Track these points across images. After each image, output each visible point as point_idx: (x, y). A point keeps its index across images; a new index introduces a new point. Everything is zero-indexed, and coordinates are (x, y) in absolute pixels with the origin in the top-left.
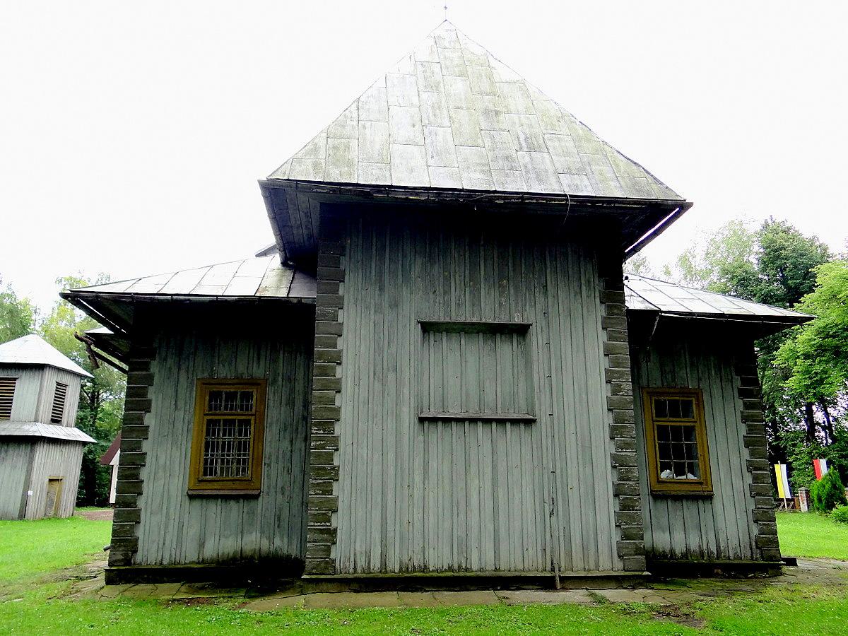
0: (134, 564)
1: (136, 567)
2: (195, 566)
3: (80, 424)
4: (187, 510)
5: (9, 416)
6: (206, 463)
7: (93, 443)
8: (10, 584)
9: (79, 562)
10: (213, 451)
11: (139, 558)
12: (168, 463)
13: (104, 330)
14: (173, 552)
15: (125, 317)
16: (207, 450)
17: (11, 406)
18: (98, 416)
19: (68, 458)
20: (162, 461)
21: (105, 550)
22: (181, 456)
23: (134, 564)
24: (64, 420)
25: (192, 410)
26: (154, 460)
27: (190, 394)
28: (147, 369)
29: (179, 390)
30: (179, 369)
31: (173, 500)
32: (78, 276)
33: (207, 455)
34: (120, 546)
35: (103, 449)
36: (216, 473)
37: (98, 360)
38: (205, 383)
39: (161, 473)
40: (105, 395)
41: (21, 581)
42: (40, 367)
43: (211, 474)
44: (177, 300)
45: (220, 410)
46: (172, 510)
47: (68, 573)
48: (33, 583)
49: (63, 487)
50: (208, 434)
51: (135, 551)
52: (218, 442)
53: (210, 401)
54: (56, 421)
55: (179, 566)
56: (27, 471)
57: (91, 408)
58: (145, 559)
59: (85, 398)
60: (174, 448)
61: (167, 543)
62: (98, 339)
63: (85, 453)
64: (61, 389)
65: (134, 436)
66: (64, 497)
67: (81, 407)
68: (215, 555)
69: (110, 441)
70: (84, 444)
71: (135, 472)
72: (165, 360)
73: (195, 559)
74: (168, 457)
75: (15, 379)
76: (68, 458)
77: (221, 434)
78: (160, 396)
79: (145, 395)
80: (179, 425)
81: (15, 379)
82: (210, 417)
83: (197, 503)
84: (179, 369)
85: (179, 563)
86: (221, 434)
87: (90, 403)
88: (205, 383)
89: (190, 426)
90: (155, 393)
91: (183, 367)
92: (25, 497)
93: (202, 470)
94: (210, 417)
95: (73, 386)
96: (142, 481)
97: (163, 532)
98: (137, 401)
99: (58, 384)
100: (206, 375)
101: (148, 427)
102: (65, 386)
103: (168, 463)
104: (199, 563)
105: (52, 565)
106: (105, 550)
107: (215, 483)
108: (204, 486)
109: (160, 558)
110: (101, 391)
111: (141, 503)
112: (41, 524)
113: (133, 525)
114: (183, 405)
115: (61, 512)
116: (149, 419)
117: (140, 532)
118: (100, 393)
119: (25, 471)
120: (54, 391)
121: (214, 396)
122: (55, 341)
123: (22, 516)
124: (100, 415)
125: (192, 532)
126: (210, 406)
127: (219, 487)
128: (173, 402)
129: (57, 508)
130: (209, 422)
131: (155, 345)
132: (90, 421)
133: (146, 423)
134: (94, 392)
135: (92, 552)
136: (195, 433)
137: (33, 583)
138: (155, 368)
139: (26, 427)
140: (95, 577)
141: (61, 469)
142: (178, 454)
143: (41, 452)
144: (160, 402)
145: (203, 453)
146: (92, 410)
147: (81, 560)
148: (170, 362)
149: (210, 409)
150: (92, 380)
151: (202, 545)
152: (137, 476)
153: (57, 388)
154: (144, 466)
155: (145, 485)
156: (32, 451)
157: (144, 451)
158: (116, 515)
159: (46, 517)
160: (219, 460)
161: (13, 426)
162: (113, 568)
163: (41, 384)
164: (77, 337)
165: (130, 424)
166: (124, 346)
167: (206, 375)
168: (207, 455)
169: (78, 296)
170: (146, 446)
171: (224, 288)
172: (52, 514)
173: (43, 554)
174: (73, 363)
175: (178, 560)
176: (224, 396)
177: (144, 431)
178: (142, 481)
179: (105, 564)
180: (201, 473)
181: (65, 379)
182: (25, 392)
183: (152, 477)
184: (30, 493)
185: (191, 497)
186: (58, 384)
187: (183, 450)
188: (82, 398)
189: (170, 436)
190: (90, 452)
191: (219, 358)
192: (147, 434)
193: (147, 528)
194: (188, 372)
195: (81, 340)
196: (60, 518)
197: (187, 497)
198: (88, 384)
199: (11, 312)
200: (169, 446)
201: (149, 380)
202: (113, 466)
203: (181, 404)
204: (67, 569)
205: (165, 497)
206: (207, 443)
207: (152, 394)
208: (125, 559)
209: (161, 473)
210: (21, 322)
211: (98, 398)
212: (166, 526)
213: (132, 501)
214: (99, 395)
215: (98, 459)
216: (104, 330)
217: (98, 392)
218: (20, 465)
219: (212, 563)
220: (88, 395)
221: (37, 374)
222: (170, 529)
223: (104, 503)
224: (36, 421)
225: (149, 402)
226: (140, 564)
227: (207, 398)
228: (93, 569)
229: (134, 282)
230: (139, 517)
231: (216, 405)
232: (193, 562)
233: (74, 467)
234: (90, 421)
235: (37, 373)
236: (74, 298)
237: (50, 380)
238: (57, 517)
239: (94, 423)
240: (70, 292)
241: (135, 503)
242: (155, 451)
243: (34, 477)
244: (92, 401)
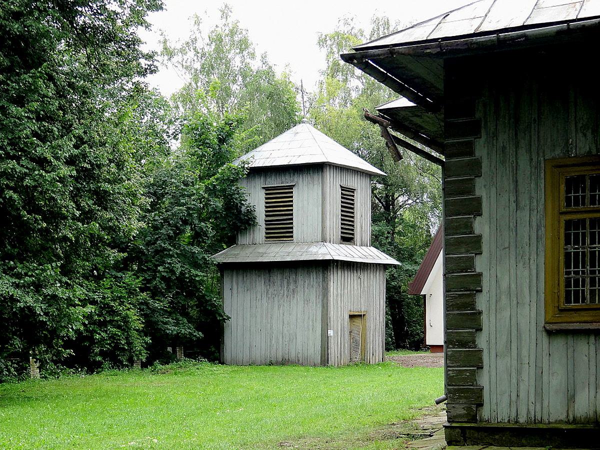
0: (481, 421)
1: (483, 425)
2: (564, 427)
3: (377, 241)
4: (546, 352)
5: (292, 237)
6: (568, 284)
7: (395, 266)
8: (333, 439)
9: (407, 417)
10: (576, 266)
11: (486, 413)
12: (513, 286)
13: (403, 102)
14: (532, 408)
15: (430, 78)
16: (568, 266)
17: (292, 223)
18: (397, 230)
19: (369, 287)
20: (504, 285)
21: (438, 402)
22: (530, 274)
23: (481, 421)
24: (357, 237)
25: (541, 207)
26: (494, 283)
27: (537, 184)
28: (471, 153)
29: (520, 181)
30: (517, 147)
31: (525, 337)
32: (343, 29)
33: (568, 273)
34: (460, 398)
35: (409, 274)
36: (584, 299)
37: (401, 149)
38: (559, 165)
39: (504, 300)
40: (401, 199)
41: (344, 437)
42: (318, 168)
43: (577, 301)
44: (505, 40)
45: (583, 204)
46: (525, 352)
47: (397, 430)
48: (358, 439)
49: (368, 324)
50: (568, 242)
51: (480, 405)
52: (583, 253)
53: (568, 191)
54: (347, 238)
55: (541, 426)
56: (323, 306)
57: (387, 219)
58: (494, 414)
59: (377, 205)
60: (520, 265)
61: (523, 395)
62: (393, 117)
63: (387, 280)
64: (347, 195)
65: (463, 250)
66: (370, 338)
67: (375, 220)
68: (591, 413)
69: (416, 263)
70: (385, 267)
71: (468, 300)
72: (495, 135)
73: (563, 417)
74: (513, 278)
75: (291, 187)
76: (369, 287)
77: (588, 240)
78: (493, 190)
79: (471, 191)
80: (524, 231)
81: (291, 187)
82: (568, 217)
83: (559, 343)
84: (517, 147)
85: (541, 422)
86: (588, 240)
87: (385, 210)
88: (559, 165)
89: (540, 233)
90: (485, 186)
91: (523, 143)
92: (325, 339)
93: (563, 294)
94: (568, 217)
95: (362, 189)
96: (480, 313)
97: (514, 381)
98: (460, 203)
99: (343, 189)
100: (558, 152)
101: (479, 238)
102: (353, 190)
103: (513, 286)
104: (568, 422)
105: (375, 418)
106: (438, 402)
107: (583, 313)
108: (566, 317)
109: (513, 415)
110: (396, 195)
111: (482, 341)
112: (348, 370)
113: (474, 371)
114: (528, 202)
115: (369, 356)
116: (481, 226)
117: (484, 380)
118: (395, 197)
119: (320, 305)
120: (339, 199)
121: (573, 184)
122: (330, 130)
123: (325, 362)
124: (399, 228)
125: (556, 381)
126: (568, 200)
127: (589, 319)
128: (513, 199)
129: (364, 351)
130: (568, 224)
131: (479, 115)
132: (387, 238)
133: (477, 231)
134: (387, 196)
135: (419, 405)
136: (549, 241)
137: (358, 439)
138: (481, 150)
139: (314, 249)
140: (431, 436)
141: (362, 301)
142: (526, 273)
143: (336, 281)
144: (493, 200)
145: (563, 270)
146: (388, 221)
147: (408, 415)
148: (503, 138)
149: (568, 204)
150: (383, 180)
151: (571, 399)
152: (472, 305)
153: (342, 194)
154: (481, 291)
155: (484, 317)
156: (325, 280)
157: (478, 270)
158: (447, 357)
159: (351, 363)
160: (588, 280)
161: (298, 248)
162: (454, 425)
163: (322, 189)
164: (368, 118)
165: (457, 234)
166: (431, 122)
167: (558, 152)
168: (568, 273)
169: (367, 56)
170: (481, 264)
171: (578, 6)
172: (359, 360)
173: (361, 407)
174: (356, 157)
175: (539, 417)
176: (588, 183)
177: (476, 243)
178: (480, 313)
179: (443, 418)
180: (562, 300)
181: (352, 182)
182: (305, 203)
183: (493, 307)
184: (331, 333)
185: (550, 333)
186: (343, 189)
187: (534, 267)
188: (374, 207)
189: (513, 248)
190: (393, 278)
191: (576, 123)
192: (480, 247)
193: (493, 373)
194: (529, 151)
195: (374, 121)
196: (368, 364)
197: (544, 334)
198: (379, 186)
199: (270, 96)
200: (513, 261)
201: (475, 168)
202: (425, 295)
203: (524, 201)
204: (393, 424)
205: (513, 334)
206: (567, 255)
207: (481, 190)
208: (468, 414)
209: (504, 300)
210: (285, 108)
211: (393, 204)
212: (519, 372)
213: (470, 339)
214: (394, 200)
215: (403, 287)
216: (403, 102)
217: (393, 196)
218: (313, 298)
219: (588, 422)
220: (380, 201)
221: (317, 177)
222: (525, 376)
223: (419, 344)
224: (324, 240)
225: (479, 200)
226: (488, 421)
227: (563, 187)
228: (426, 426)
229: (438, 20)
230: (481, 360)
231: (576, 198)
232: (561, 422)
233: (356, 300)
234: (387, 238)
235: (316, 176)
236: (360, 58)
237: (333, 183)
238: (364, 362)
239: (393, 239)
240: (354, 52)
241: (474, 342)
242: (493, 270)
243: (332, 313)
244: (387, 208)
